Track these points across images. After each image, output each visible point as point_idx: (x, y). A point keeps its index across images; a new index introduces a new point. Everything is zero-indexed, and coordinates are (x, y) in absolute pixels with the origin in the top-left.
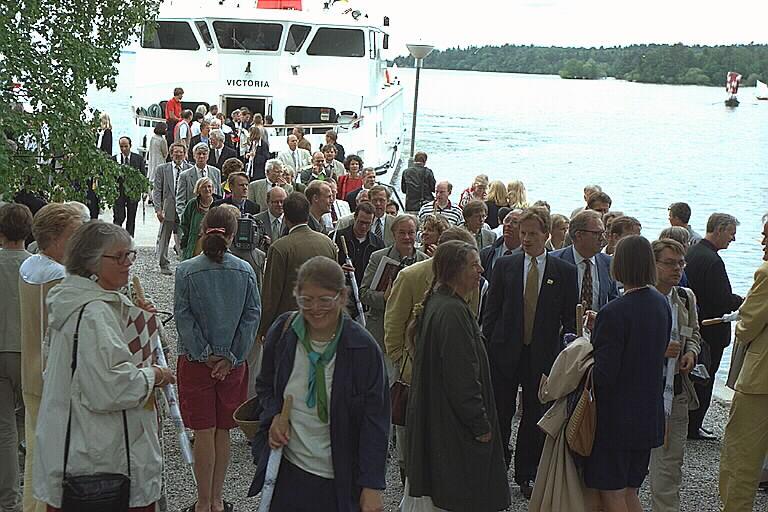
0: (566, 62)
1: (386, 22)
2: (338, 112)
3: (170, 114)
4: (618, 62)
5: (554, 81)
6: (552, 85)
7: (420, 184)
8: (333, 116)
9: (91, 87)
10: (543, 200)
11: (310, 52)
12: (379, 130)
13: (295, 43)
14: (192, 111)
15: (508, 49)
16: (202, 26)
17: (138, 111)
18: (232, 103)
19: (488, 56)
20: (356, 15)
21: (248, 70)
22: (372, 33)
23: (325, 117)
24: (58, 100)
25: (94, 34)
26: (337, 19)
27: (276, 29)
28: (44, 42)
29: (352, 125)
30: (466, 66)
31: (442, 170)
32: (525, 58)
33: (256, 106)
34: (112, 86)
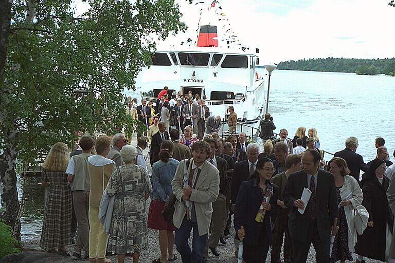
0: (360, 66)
1: (257, 51)
2: (235, 94)
3: (161, 95)
4: (386, 67)
5: (353, 76)
6: (351, 78)
7: (267, 127)
8: (233, 96)
9: (126, 89)
10: (285, 129)
11: (222, 66)
12: (254, 102)
13: (215, 63)
14: (170, 93)
15: (329, 60)
16: (173, 55)
17: (143, 94)
18: (186, 90)
19: (319, 64)
20: (243, 49)
21: (194, 75)
22: (251, 57)
23: (229, 96)
24: (111, 94)
25: (127, 66)
26: (235, 50)
27: (207, 56)
28: (106, 70)
29: (242, 100)
30: (308, 69)
31: (280, 123)
32: (338, 65)
33: (197, 92)
34: (134, 88)
